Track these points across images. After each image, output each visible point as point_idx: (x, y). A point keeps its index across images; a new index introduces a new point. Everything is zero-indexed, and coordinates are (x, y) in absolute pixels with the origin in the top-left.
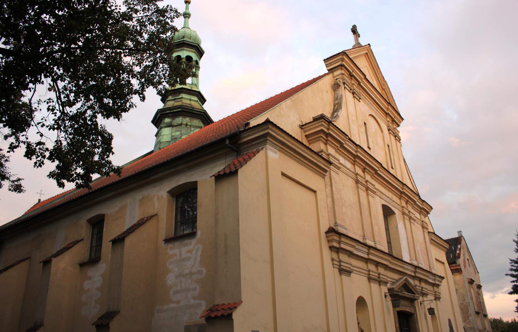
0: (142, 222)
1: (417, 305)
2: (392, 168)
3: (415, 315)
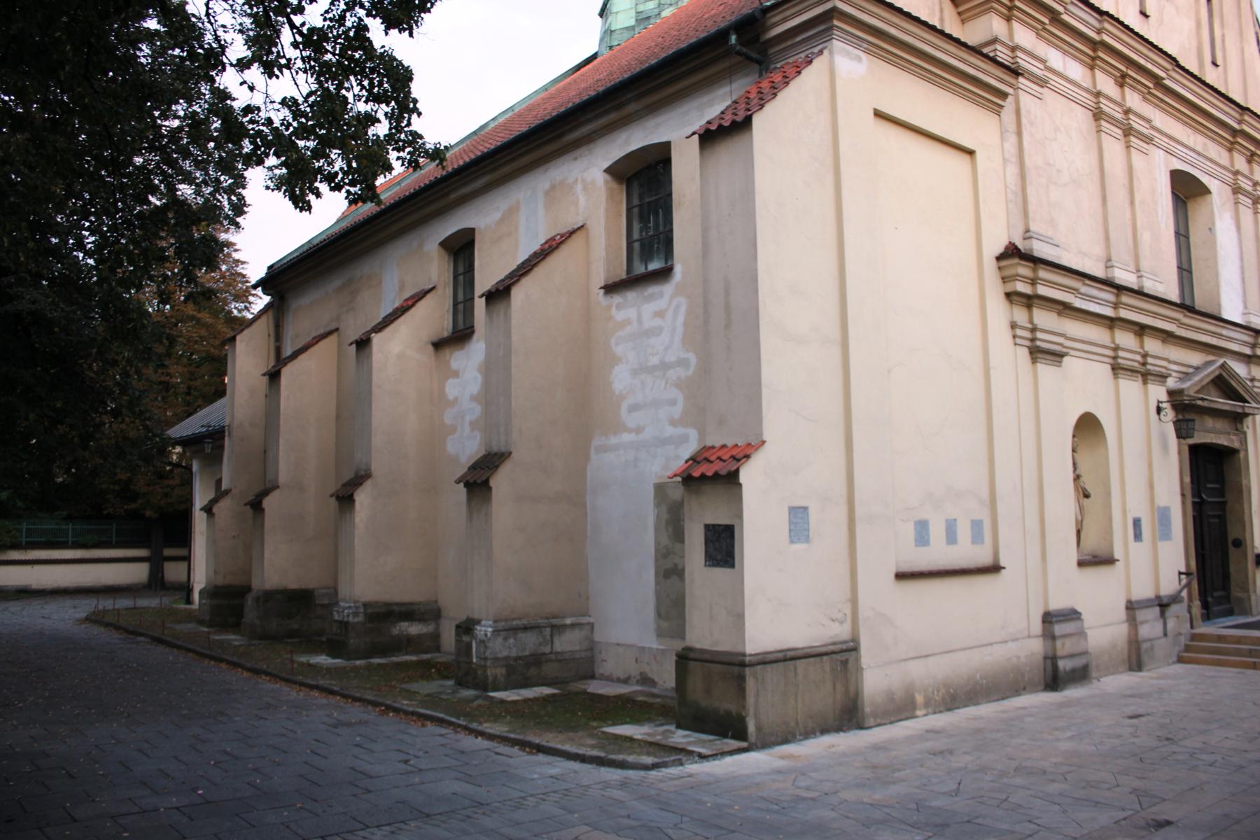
0: (550, 247)
1: (1251, 427)
2: (1215, 64)
3: (1242, 455)
